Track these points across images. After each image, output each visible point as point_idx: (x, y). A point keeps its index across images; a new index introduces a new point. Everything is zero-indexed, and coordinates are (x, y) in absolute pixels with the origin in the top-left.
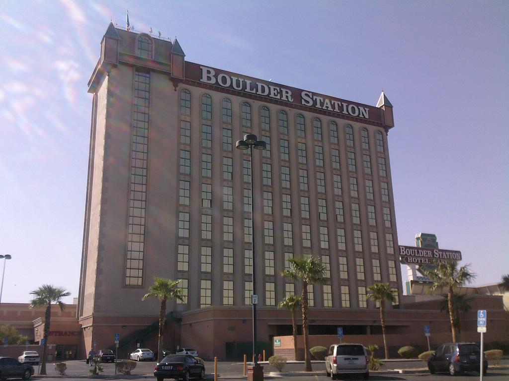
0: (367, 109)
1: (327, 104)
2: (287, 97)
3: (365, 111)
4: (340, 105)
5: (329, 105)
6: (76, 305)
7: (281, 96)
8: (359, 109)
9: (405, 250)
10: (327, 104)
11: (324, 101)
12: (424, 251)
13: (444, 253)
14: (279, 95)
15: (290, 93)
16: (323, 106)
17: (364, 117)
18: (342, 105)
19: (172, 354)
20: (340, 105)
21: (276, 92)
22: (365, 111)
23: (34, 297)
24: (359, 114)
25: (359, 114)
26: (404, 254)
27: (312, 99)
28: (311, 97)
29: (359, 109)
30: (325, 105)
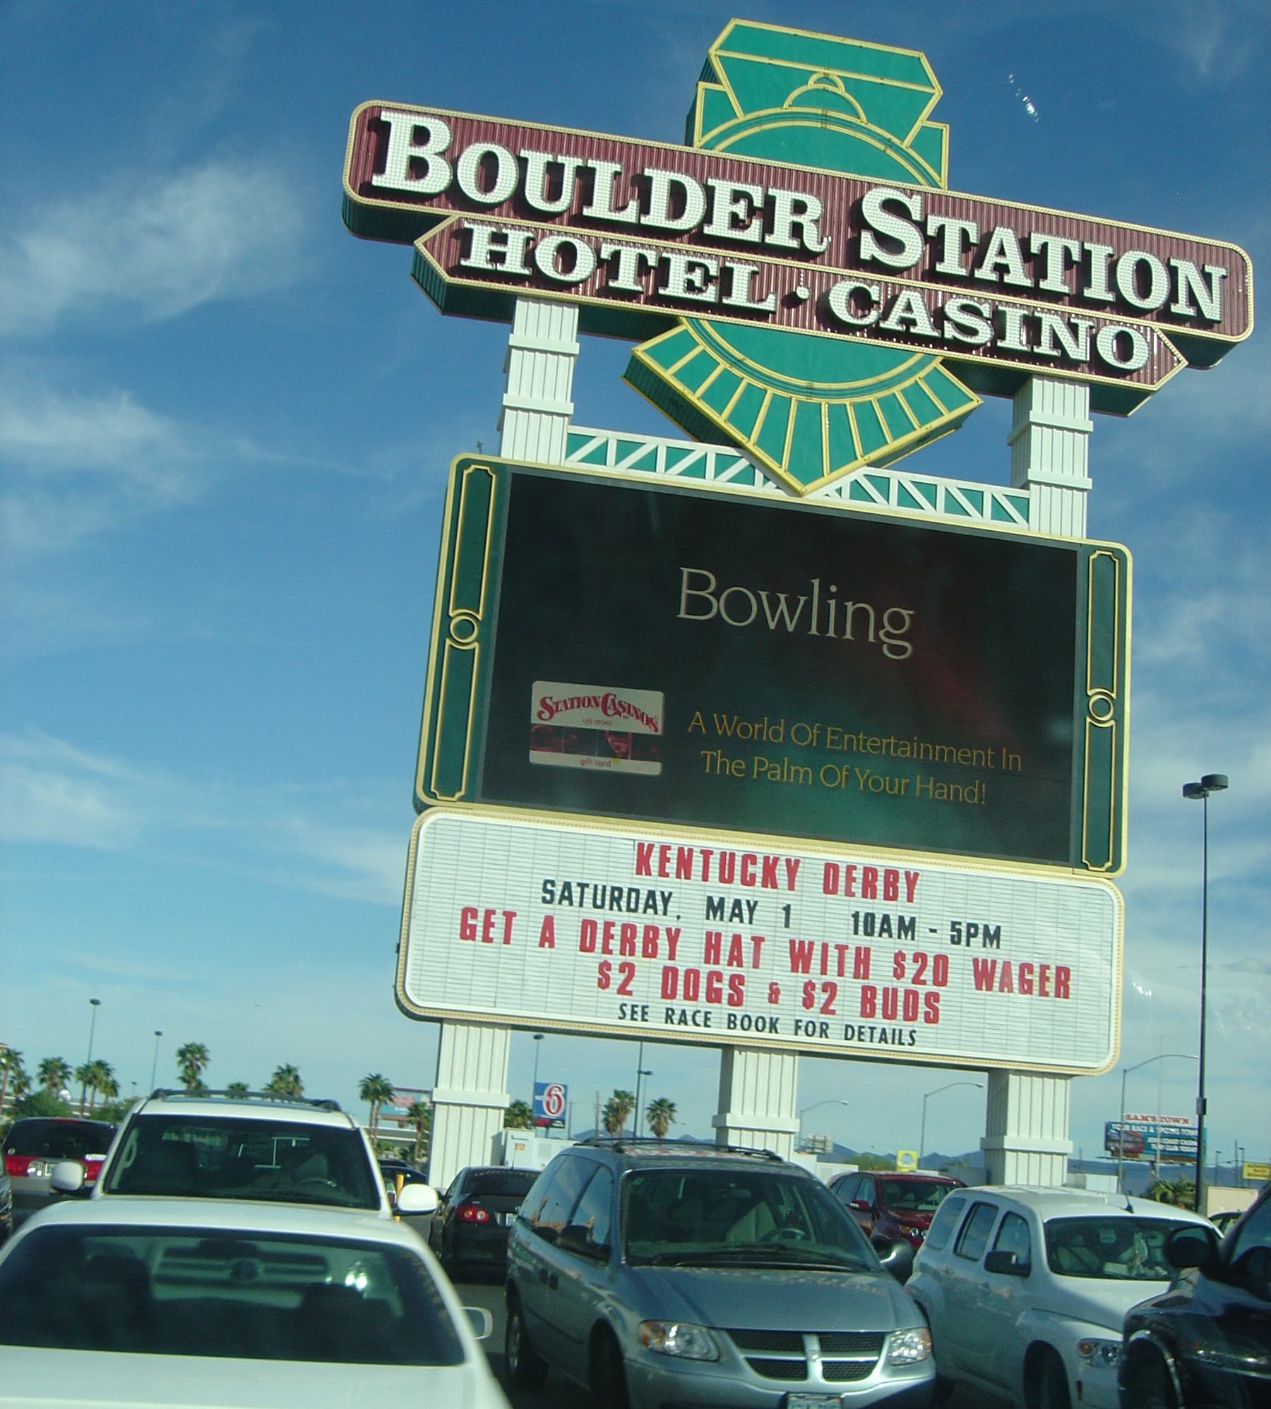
0: (1217, 272)
1: (1002, 252)
2: (797, 230)
3: (1207, 278)
4: (1076, 257)
5: (1013, 258)
6: (1001, 1182)
7: (768, 228)
8: (1173, 272)
9: (452, 157)
10: (1002, 252)
11: (986, 238)
12: (723, 189)
13: (1004, 236)
14: (756, 224)
15: (814, 207)
16: (978, 262)
17: (1199, 311)
18: (1086, 255)
19: (989, 1254)
20: (1076, 257)
21: (741, 209)
22: (1207, 278)
23: (182, 1067)
24: (1173, 297)
25: (1173, 297)
26: (436, 180)
27: (922, 226)
28: (916, 216)
29: (1173, 272)
30: (991, 258)
